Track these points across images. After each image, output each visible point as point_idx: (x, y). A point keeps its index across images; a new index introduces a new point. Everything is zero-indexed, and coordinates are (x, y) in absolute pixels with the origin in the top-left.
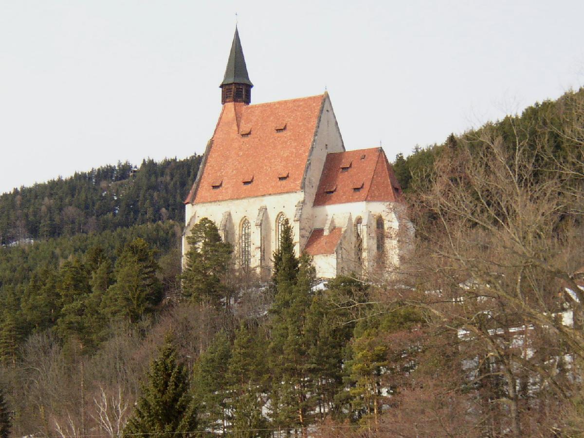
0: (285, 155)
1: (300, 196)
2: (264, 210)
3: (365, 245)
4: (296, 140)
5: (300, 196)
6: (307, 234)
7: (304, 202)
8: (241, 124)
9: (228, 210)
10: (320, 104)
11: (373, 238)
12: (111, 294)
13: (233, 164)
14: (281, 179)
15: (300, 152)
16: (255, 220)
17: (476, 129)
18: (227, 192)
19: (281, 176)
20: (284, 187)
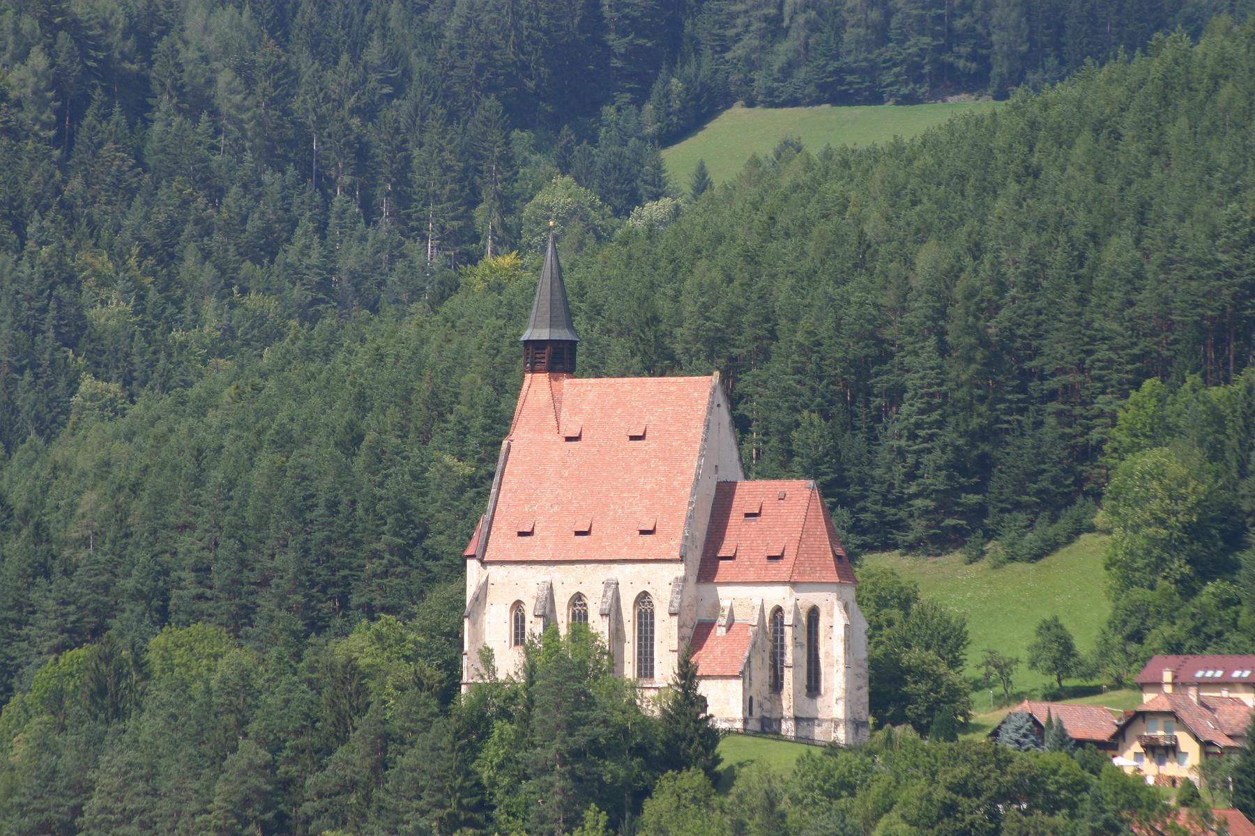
0: (648, 487)
1: (679, 570)
2: (614, 588)
3: (789, 659)
4: (664, 459)
5: (679, 570)
6: (689, 632)
7: (685, 580)
8: (562, 415)
9: (548, 579)
10: (707, 394)
11: (802, 645)
12: (56, 493)
13: (552, 491)
14: (643, 532)
15: (675, 483)
16: (599, 604)
17: (828, 106)
18: (546, 547)
19: (643, 528)
20: (650, 549)
